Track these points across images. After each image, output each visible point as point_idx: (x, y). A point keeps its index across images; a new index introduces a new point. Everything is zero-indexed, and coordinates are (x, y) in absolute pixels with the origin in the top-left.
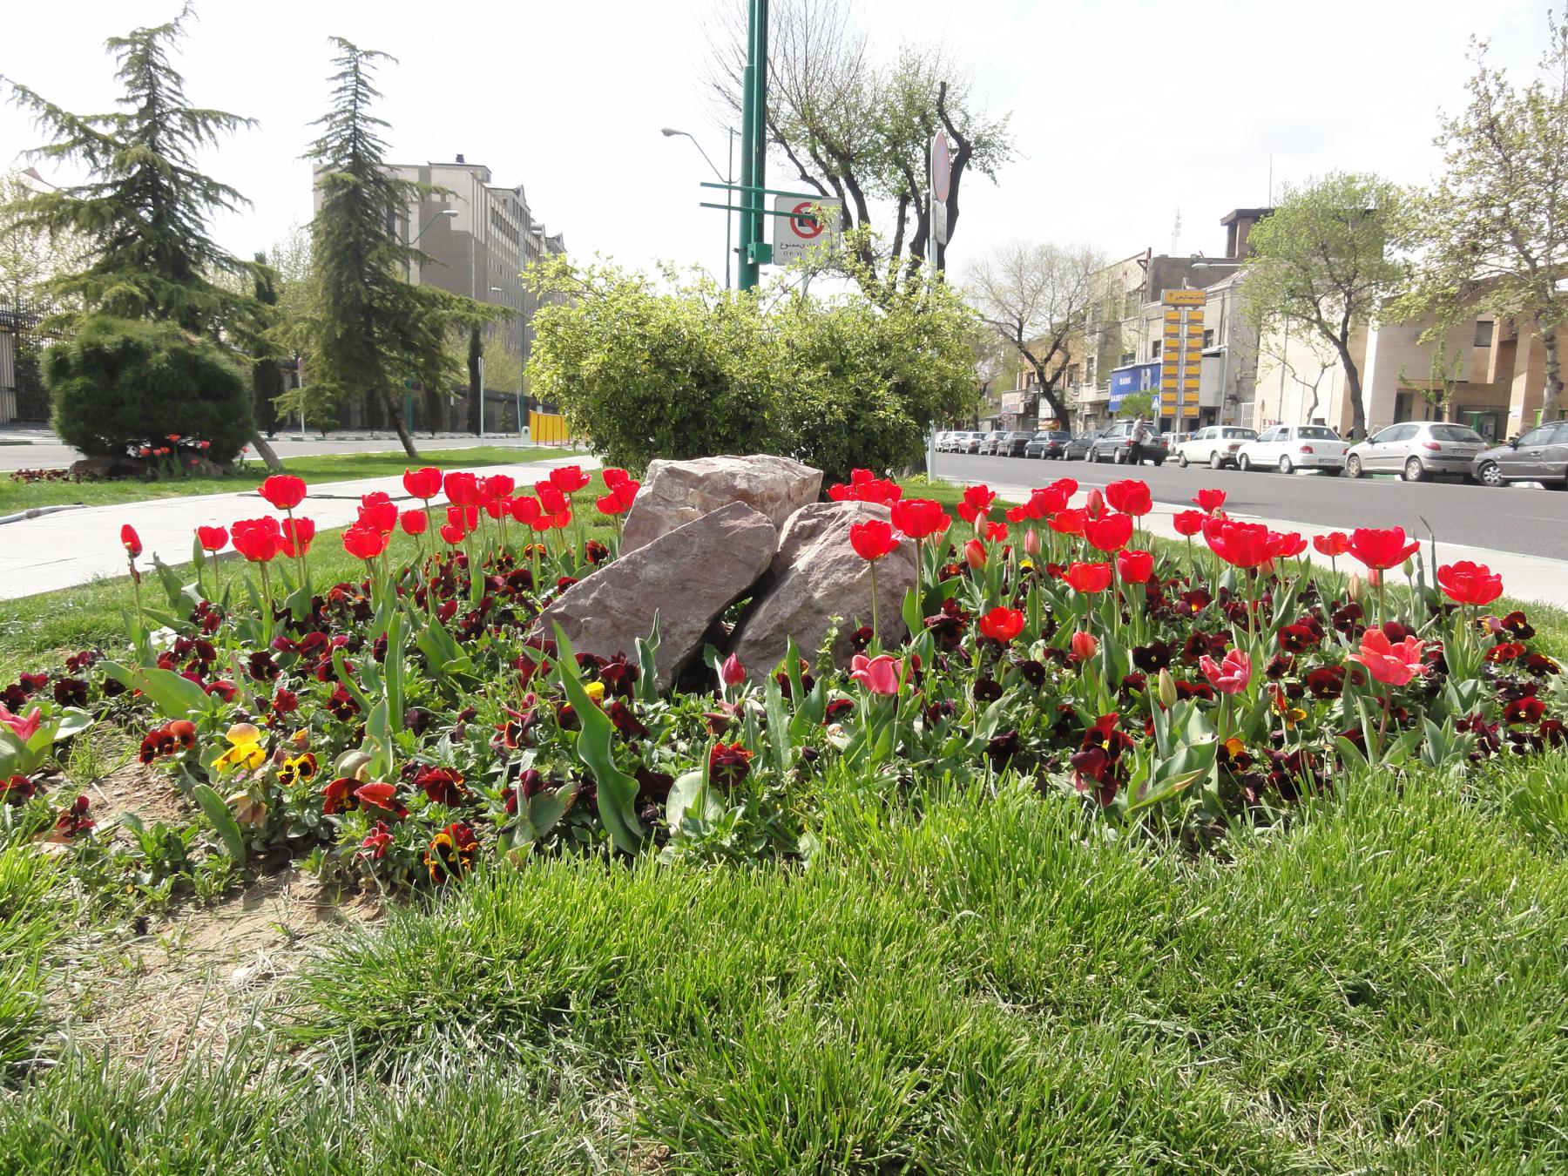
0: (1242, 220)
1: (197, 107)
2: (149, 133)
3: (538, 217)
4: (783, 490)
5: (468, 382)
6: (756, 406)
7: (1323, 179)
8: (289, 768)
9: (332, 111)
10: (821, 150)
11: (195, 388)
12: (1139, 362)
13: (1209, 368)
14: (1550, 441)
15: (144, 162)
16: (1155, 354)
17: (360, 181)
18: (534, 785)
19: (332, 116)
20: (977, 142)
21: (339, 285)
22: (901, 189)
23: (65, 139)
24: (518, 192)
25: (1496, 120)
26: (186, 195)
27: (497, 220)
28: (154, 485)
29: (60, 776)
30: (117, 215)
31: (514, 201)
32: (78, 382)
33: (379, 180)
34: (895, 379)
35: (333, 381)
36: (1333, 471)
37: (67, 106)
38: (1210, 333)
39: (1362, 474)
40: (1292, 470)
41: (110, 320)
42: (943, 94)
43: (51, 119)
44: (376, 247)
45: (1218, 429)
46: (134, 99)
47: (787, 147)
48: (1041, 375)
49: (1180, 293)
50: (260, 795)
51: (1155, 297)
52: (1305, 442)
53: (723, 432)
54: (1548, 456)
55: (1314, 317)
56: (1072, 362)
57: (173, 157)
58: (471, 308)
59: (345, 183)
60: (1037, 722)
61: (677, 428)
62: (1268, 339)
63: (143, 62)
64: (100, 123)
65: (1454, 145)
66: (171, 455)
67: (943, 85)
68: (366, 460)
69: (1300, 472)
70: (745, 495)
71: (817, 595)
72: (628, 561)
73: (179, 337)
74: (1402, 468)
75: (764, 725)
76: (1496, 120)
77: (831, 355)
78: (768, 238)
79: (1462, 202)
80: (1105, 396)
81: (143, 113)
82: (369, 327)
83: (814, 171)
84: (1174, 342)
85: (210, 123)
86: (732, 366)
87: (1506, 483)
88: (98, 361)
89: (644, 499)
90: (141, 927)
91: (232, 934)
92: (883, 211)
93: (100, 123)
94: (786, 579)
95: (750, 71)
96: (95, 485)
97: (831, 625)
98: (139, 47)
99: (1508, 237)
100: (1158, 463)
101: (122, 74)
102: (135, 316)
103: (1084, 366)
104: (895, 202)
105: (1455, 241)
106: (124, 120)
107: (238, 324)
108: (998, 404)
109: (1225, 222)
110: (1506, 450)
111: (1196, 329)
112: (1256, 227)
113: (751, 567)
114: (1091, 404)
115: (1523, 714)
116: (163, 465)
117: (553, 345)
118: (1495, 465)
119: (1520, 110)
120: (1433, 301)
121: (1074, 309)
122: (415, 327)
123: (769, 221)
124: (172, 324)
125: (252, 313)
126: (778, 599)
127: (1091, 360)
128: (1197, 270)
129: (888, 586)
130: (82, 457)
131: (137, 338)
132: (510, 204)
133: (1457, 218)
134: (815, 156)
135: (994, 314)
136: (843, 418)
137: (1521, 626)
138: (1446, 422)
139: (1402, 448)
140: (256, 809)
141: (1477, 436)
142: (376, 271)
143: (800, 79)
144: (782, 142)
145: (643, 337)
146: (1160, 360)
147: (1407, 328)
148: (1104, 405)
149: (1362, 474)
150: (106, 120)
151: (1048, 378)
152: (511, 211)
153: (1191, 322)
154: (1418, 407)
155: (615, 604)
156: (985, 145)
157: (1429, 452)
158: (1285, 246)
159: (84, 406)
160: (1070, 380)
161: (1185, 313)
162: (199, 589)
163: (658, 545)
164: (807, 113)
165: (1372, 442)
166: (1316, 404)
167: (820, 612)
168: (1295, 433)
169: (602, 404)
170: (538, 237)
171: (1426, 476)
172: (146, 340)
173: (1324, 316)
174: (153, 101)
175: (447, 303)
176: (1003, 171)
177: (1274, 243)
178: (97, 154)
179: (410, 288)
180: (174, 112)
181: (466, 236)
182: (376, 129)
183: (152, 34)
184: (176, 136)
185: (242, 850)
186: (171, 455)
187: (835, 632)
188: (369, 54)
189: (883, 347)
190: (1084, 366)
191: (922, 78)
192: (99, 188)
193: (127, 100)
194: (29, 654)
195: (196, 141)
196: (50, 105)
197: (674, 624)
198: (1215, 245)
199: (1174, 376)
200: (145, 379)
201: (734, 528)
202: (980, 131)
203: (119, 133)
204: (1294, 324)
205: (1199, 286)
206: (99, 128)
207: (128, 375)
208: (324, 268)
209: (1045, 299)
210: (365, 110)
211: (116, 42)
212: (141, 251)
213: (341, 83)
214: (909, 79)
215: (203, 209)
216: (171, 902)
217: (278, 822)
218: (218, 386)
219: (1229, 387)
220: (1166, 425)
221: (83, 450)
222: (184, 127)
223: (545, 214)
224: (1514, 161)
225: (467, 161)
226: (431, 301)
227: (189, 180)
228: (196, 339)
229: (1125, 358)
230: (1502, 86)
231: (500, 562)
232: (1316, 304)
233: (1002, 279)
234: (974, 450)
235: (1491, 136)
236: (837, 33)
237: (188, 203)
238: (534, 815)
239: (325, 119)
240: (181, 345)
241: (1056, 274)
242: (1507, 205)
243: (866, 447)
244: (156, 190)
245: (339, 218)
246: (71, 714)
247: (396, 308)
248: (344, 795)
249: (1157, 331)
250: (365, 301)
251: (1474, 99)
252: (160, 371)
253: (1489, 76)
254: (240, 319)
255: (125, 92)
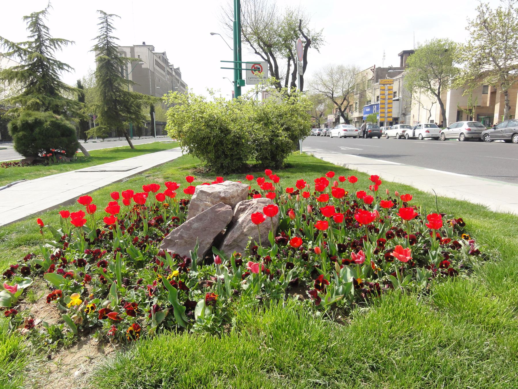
0: (405, 54)
1: (54, 38)
2: (39, 47)
3: (171, 61)
4: (236, 194)
5: (150, 119)
6: (240, 138)
7: (430, 41)
8: (88, 308)
9: (99, 35)
10: (261, 43)
11: (59, 133)
12: (372, 103)
13: (395, 105)
14: (506, 127)
15: (37, 57)
16: (378, 100)
17: (110, 58)
18: (157, 309)
19: (100, 37)
20: (312, 39)
21: (105, 93)
22: (288, 55)
23: (11, 50)
24: (164, 54)
25: (486, 20)
26: (52, 67)
27: (157, 64)
28: (47, 167)
29: (24, 301)
30: (30, 75)
31: (163, 57)
32: (21, 133)
33: (116, 57)
34: (285, 126)
35: (105, 125)
36: (436, 138)
37: (11, 40)
38: (395, 93)
39: (446, 139)
40: (423, 139)
41: (30, 112)
42: (300, 24)
43: (6, 45)
44: (117, 80)
45: (398, 126)
46: (33, 36)
47: (250, 43)
48: (340, 109)
49: (385, 80)
50: (80, 315)
51: (377, 82)
52: (427, 129)
53: (230, 147)
54: (505, 131)
55: (429, 87)
56: (350, 104)
57: (47, 54)
58: (149, 99)
59: (105, 59)
60: (305, 273)
61: (215, 146)
62: (415, 95)
63: (36, 23)
64: (23, 45)
65: (472, 29)
66: (53, 156)
67: (300, 20)
68: (117, 151)
69: (426, 139)
70: (223, 199)
71: (245, 230)
72: (188, 223)
73: (53, 117)
74: (458, 137)
75: (223, 283)
76: (486, 20)
77: (264, 120)
78: (244, 77)
79: (475, 48)
80: (361, 115)
81: (36, 41)
82: (116, 106)
83: (259, 50)
84: (383, 97)
85: (59, 43)
86: (232, 127)
87: (492, 141)
88: (26, 126)
89: (194, 199)
90: (49, 357)
91: (74, 358)
92: (282, 63)
93: (23, 45)
94: (236, 225)
95: (235, 23)
96: (29, 167)
97: (249, 240)
98: (34, 18)
99: (491, 59)
100: (379, 138)
101: (29, 28)
102: (38, 110)
103: (354, 105)
104: (287, 59)
105: (474, 61)
106: (30, 43)
107: (73, 110)
108: (327, 119)
109: (399, 55)
110: (492, 130)
111: (390, 92)
112: (409, 58)
113: (225, 222)
114: (357, 118)
115: (444, 265)
116: (50, 159)
117: (174, 121)
118: (488, 135)
119: (494, 16)
120: (467, 81)
121: (350, 86)
122: (131, 106)
123: (244, 73)
124: (51, 113)
125: (76, 105)
126: (233, 232)
127: (356, 103)
128: (390, 73)
129: (266, 226)
130: (24, 158)
131: (39, 118)
132: (161, 58)
133: (474, 54)
134: (259, 45)
135: (324, 89)
136: (268, 140)
137: (461, 222)
138: (473, 121)
139: (458, 130)
140: (80, 319)
141: (483, 125)
142: (117, 88)
143: (253, 20)
144: (248, 41)
145: (202, 118)
146: (379, 102)
147: (458, 92)
148: (362, 118)
149: (446, 139)
150: (25, 44)
151: (343, 110)
152: (162, 60)
153: (389, 90)
154: (464, 116)
155: (185, 236)
156: (315, 40)
157: (467, 131)
158: (418, 64)
159: (24, 141)
160: (350, 110)
161: (386, 87)
162: (62, 231)
163: (197, 217)
164: (256, 33)
165: (449, 129)
166: (430, 116)
167: (246, 235)
168: (424, 126)
169: (191, 140)
170: (171, 69)
171: (466, 139)
172: (42, 118)
173: (432, 86)
174: (39, 36)
175: (141, 98)
176: (321, 48)
177: (415, 63)
178: (22, 55)
179: (129, 93)
180: (47, 40)
181: (147, 69)
182: (115, 41)
183: (38, 14)
184: (48, 48)
185: (76, 331)
186: (53, 156)
187: (250, 242)
188: (111, 15)
189: (280, 116)
190: (354, 105)
191: (294, 18)
192: (23, 66)
193: (31, 37)
194: (12, 249)
195: (55, 49)
196: (6, 40)
197: (203, 241)
198: (396, 63)
199: (384, 108)
200: (43, 131)
201: (219, 211)
202: (313, 35)
203: (29, 48)
204: (422, 90)
205: (392, 77)
206: (22, 46)
207: (37, 130)
208: (100, 88)
209: (340, 83)
210: (110, 34)
211: (26, 17)
212: (39, 87)
213: (102, 25)
214: (289, 18)
215: (59, 72)
216: (58, 348)
217: (86, 321)
218: (67, 132)
219: (402, 110)
220: (382, 124)
221: (24, 155)
222: (50, 45)
223: (174, 61)
224: (493, 33)
225: (146, 44)
226: (136, 97)
227: (53, 62)
228: (59, 117)
229: (368, 102)
230: (488, 9)
231: (154, 210)
232: (429, 83)
233: (326, 78)
234: (319, 135)
235: (485, 26)
236: (265, 4)
237: (53, 70)
238: (157, 319)
239: (97, 38)
240: (54, 119)
241: (344, 75)
242: (491, 48)
243: (277, 149)
244: (42, 66)
245: (104, 71)
246: (26, 280)
247: (126, 99)
248: (105, 313)
249: (378, 93)
250: (114, 98)
251: (479, 13)
252: (48, 129)
253: (483, 5)
254: (73, 108)
255: (30, 34)
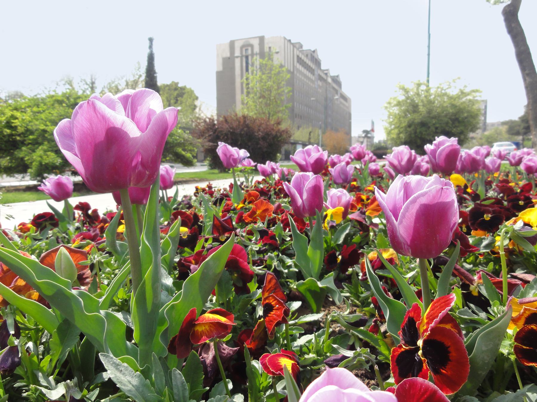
170: (326, 74)
223: (330, 64)
